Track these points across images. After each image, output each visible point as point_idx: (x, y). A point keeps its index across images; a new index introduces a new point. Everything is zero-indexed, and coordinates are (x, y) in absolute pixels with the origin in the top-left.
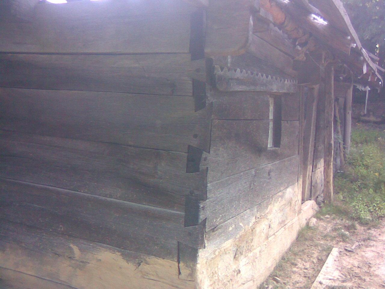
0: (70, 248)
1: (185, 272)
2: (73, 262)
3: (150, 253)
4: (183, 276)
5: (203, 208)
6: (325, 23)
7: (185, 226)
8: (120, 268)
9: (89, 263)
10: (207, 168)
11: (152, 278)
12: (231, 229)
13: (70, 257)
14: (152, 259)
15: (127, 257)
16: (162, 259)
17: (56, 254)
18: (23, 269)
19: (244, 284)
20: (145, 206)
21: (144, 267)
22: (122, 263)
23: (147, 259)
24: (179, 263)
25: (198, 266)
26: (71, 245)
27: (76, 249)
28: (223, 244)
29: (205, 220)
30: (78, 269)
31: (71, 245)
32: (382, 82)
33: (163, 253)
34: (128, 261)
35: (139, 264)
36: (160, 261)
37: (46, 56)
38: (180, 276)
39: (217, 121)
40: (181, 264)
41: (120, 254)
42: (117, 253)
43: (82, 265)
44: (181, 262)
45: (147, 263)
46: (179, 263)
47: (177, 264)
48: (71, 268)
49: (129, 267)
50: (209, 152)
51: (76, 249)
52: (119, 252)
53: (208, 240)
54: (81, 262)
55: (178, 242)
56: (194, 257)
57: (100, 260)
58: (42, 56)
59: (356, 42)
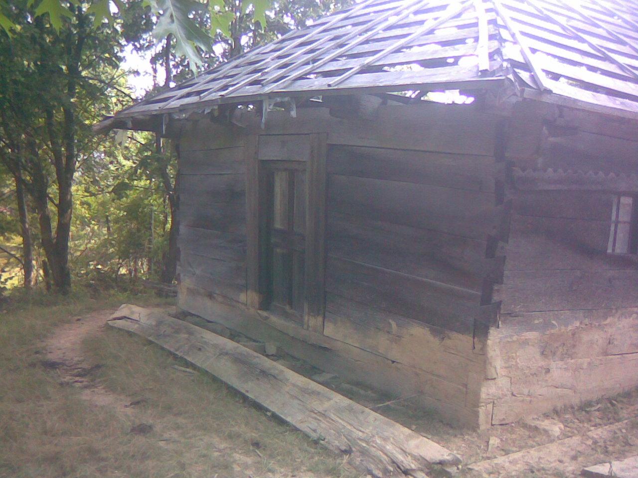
0: (390, 323)
1: (478, 346)
4: (476, 351)
5: (498, 291)
7: (481, 305)
9: (403, 337)
10: (505, 256)
11: (452, 352)
12: (536, 322)
13: (388, 332)
14: (454, 335)
15: (434, 332)
16: (461, 335)
17: (377, 329)
18: (349, 341)
19: (557, 387)
21: (448, 342)
22: (431, 338)
23: (450, 334)
24: (474, 338)
25: (489, 342)
26: (390, 321)
27: (393, 324)
28: (525, 333)
29: (500, 302)
31: (390, 321)
32: (133, 110)
33: (463, 329)
35: (443, 339)
36: (460, 336)
37: (383, 150)
40: (476, 339)
41: (429, 329)
42: (427, 329)
43: (397, 339)
44: (476, 337)
45: (450, 338)
46: (474, 338)
47: (472, 339)
48: (388, 341)
49: (434, 341)
50: (507, 242)
51: (393, 324)
53: (504, 322)
54: (397, 336)
55: (475, 319)
56: (486, 334)
57: (412, 335)
58: (380, 150)
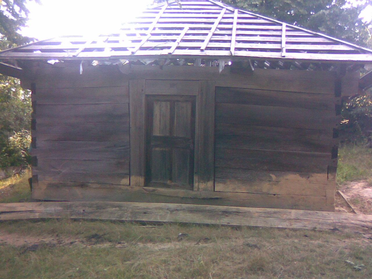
2: (271, 182)
3: (314, 172)
6: (81, 73)
8: (298, 181)
15: (302, 175)
20: (312, 153)
21: (311, 178)
23: (313, 175)
26: (271, 175)
30: (356, 7)
31: (271, 175)
34: (303, 177)
35: (309, 177)
36: (319, 175)
37: (260, 91)
38: (328, 179)
39: (276, 3)
40: (329, 175)
45: (312, 176)
47: (327, 175)
49: (303, 180)
52: (298, 174)
59: (32, 50)
